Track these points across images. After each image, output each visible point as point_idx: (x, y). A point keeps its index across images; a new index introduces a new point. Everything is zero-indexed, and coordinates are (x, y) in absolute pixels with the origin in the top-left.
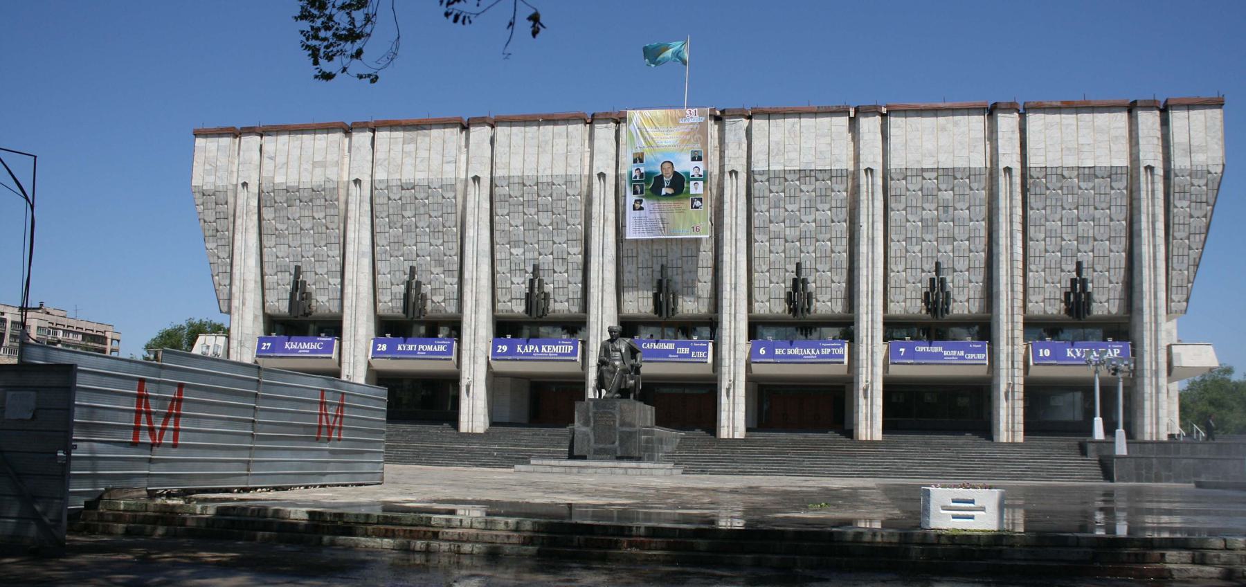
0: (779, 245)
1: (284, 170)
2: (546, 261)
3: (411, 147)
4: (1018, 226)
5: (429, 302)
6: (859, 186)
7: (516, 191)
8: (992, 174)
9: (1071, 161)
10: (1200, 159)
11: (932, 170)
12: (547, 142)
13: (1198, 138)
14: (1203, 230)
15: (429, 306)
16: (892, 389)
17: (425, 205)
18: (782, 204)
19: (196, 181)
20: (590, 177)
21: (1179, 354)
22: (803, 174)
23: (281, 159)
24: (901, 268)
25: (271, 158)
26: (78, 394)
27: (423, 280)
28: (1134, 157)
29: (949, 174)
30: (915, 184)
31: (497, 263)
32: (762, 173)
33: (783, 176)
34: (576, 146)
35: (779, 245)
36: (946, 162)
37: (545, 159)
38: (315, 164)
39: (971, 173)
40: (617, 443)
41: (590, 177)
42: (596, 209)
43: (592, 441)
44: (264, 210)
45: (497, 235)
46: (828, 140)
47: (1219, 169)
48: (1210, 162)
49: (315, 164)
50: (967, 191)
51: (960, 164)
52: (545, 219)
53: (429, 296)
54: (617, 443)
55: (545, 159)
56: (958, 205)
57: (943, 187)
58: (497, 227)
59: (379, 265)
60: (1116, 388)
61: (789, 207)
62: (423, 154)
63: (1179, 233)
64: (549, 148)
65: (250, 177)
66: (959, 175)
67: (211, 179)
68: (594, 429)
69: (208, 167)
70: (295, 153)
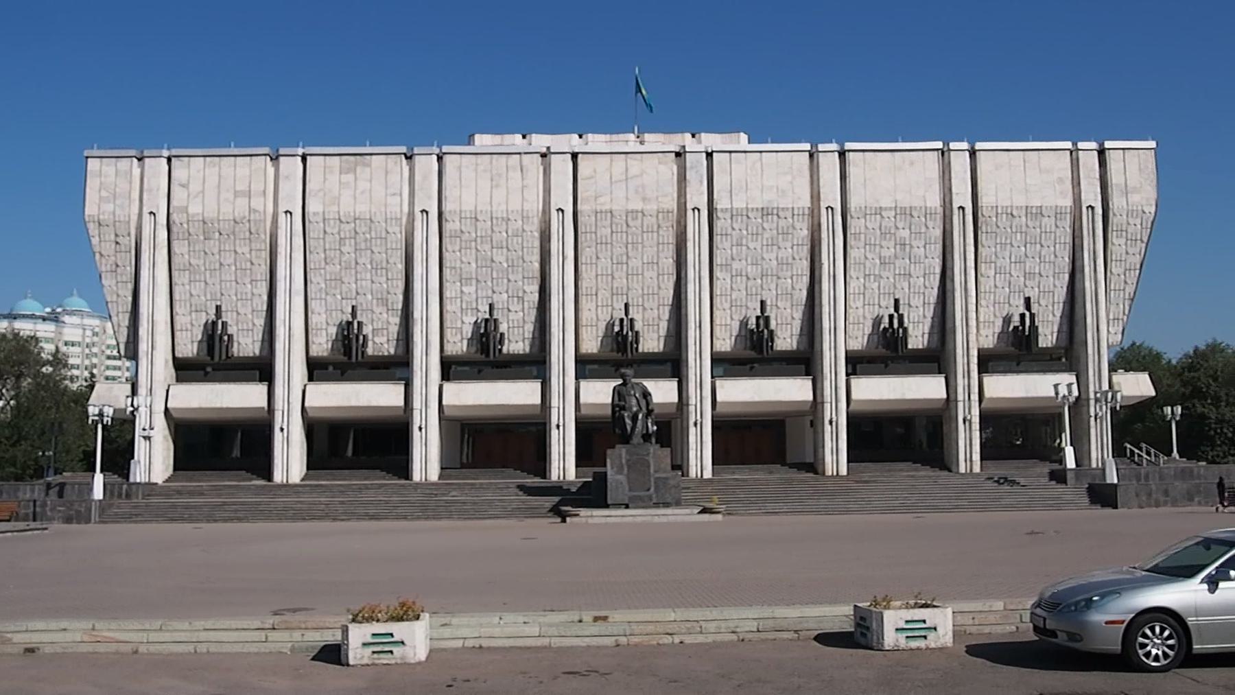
0: (740, 282)
1: (199, 199)
2: (500, 300)
3: (349, 177)
4: (971, 263)
5: (370, 344)
6: (819, 225)
7: (467, 226)
8: (814, 212)
9: (1020, 201)
10: (1135, 198)
11: (891, 209)
12: (500, 175)
13: (1134, 179)
14: (1138, 266)
15: (235, 350)
16: (855, 421)
17: (366, 240)
18: (744, 242)
19: (90, 209)
20: (411, 215)
21: (1119, 384)
22: (765, 212)
23: (195, 187)
24: (860, 304)
25: (183, 186)
26: (154, 480)
27: (364, 320)
28: (816, 196)
29: (906, 213)
30: (873, 223)
31: (447, 302)
32: (724, 211)
33: (746, 214)
34: (394, 178)
35: (740, 282)
36: (905, 201)
37: (499, 195)
38: (236, 194)
39: (927, 213)
40: (652, 489)
41: (411, 215)
42: (555, 246)
43: (627, 488)
44: (175, 244)
45: (447, 272)
46: (789, 178)
47: (1153, 210)
48: (1144, 202)
49: (236, 194)
50: (923, 230)
51: (917, 203)
52: (500, 257)
53: (370, 337)
54: (652, 489)
55: (499, 195)
56: (914, 243)
57: (900, 225)
58: (447, 263)
59: (313, 304)
60: (1061, 415)
61: (751, 245)
62: (363, 185)
63: (1115, 268)
64: (503, 182)
65: (158, 207)
66: (915, 214)
67: (110, 207)
68: (628, 478)
69: (104, 194)
70: (212, 181)
